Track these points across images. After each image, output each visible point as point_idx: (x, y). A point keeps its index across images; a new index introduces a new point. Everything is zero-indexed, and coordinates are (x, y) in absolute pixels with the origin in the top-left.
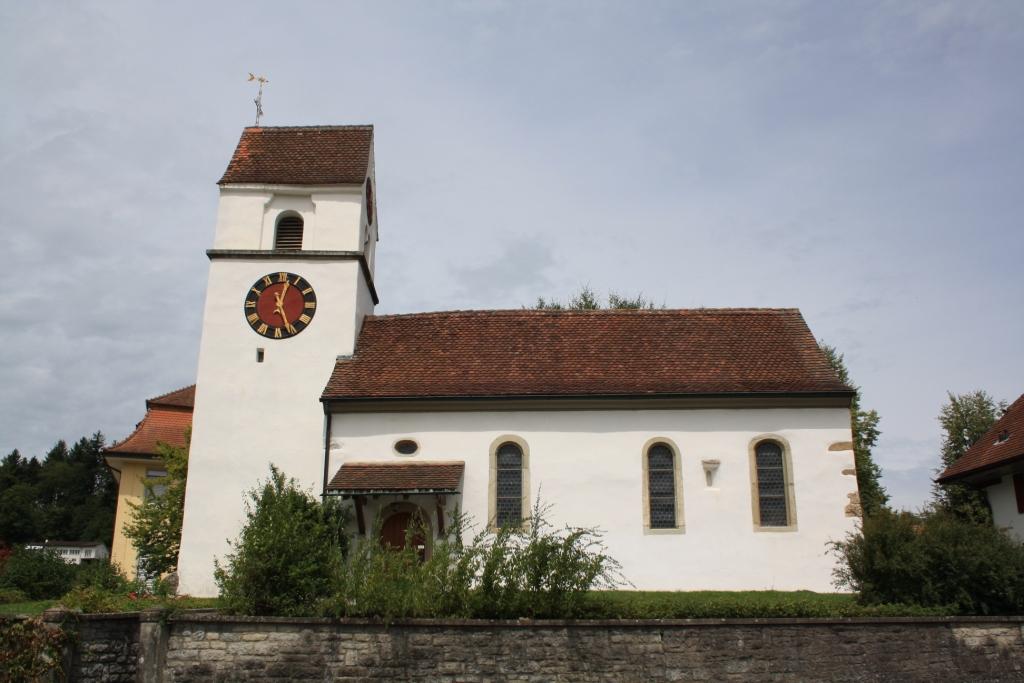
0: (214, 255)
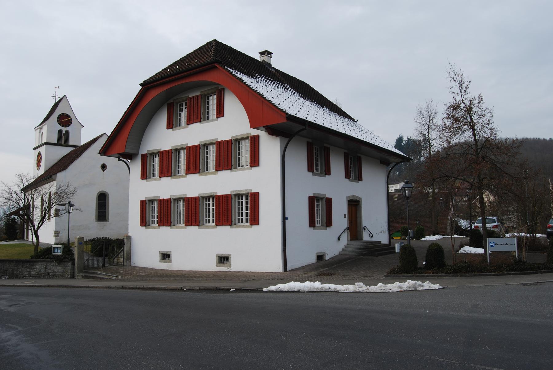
0: (34, 149)
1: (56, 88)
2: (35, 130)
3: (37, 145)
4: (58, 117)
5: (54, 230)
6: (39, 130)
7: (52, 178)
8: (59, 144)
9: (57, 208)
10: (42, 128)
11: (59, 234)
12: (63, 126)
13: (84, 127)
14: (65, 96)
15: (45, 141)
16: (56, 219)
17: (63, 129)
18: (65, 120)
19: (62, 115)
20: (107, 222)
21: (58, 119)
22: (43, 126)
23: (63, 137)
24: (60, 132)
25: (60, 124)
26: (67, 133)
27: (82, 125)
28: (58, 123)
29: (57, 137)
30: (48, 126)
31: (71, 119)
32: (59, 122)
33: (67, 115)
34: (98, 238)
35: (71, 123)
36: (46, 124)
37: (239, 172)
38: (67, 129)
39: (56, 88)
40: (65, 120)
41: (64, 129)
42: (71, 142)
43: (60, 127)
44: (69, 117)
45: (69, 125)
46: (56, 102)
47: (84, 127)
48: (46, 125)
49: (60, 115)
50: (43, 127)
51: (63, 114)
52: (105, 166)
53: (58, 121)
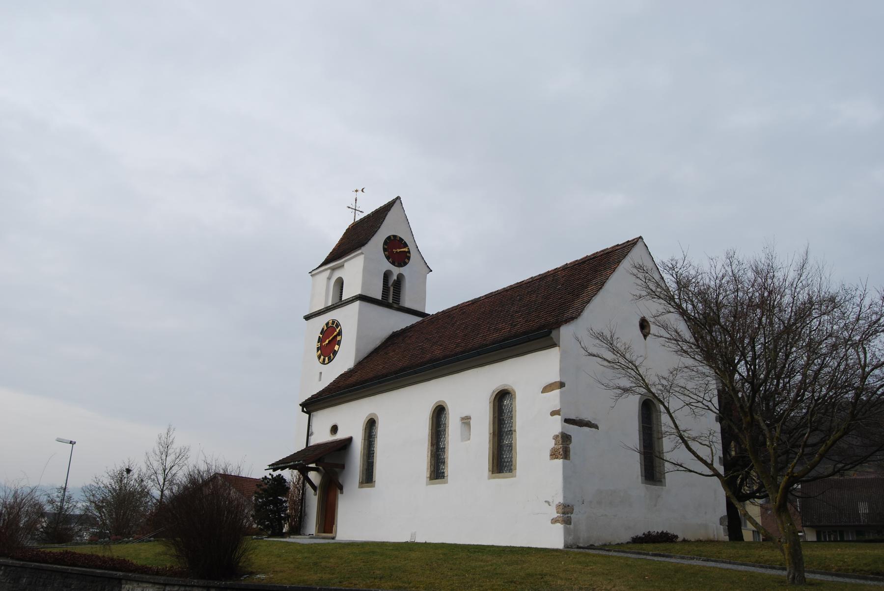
0: (307, 318)
1: (357, 191)
2: (311, 275)
3: (321, 306)
4: (385, 243)
5: (560, 499)
6: (329, 271)
7: (552, 338)
8: (382, 303)
9: (563, 431)
10: (343, 265)
11: (572, 516)
12: (393, 263)
13: (431, 271)
14: (398, 198)
15: (358, 291)
16: (563, 462)
17: (393, 271)
18: (398, 250)
19: (392, 238)
20: (662, 485)
21: (386, 247)
22: (346, 261)
23: (392, 289)
24: (387, 275)
25: (388, 258)
26: (400, 277)
27: (428, 267)
28: (385, 255)
29: (382, 285)
30: (365, 258)
31: (409, 252)
32: (386, 253)
33: (401, 240)
34: (658, 532)
35: (409, 258)
36: (362, 253)
37: (449, 449)
38: (402, 270)
39: (357, 191)
40: (398, 250)
41: (396, 271)
42: (407, 303)
43: (387, 265)
44: (406, 245)
45: (405, 264)
46: (357, 219)
47: (431, 271)
48: (362, 257)
49: (389, 238)
50: (346, 265)
51: (395, 236)
52: (646, 324)
53: (385, 250)
